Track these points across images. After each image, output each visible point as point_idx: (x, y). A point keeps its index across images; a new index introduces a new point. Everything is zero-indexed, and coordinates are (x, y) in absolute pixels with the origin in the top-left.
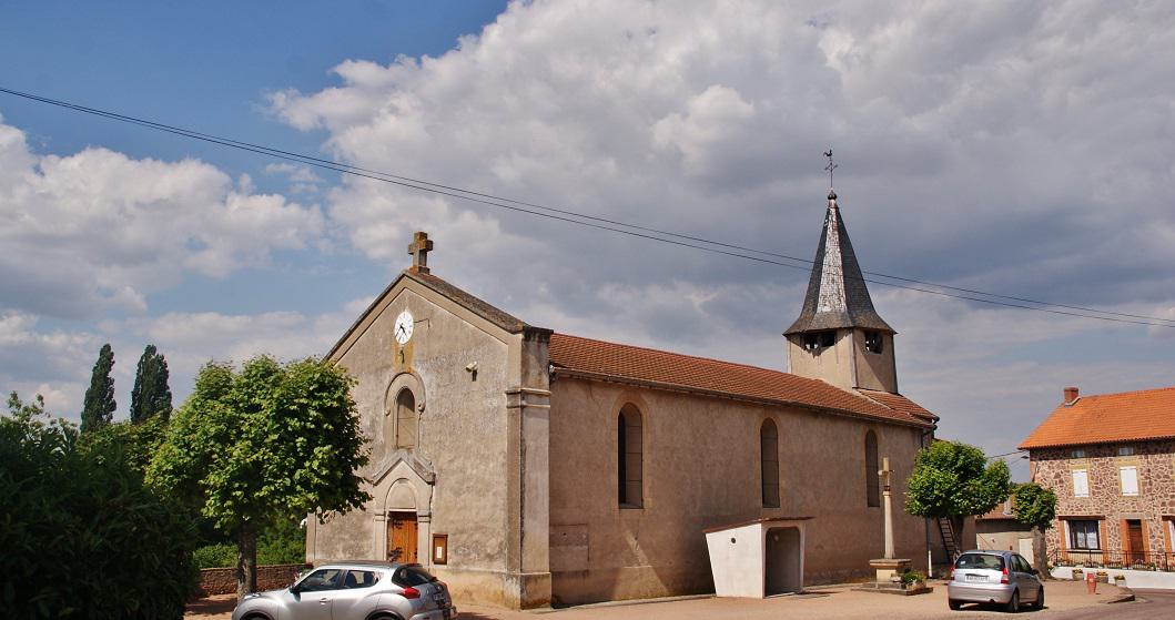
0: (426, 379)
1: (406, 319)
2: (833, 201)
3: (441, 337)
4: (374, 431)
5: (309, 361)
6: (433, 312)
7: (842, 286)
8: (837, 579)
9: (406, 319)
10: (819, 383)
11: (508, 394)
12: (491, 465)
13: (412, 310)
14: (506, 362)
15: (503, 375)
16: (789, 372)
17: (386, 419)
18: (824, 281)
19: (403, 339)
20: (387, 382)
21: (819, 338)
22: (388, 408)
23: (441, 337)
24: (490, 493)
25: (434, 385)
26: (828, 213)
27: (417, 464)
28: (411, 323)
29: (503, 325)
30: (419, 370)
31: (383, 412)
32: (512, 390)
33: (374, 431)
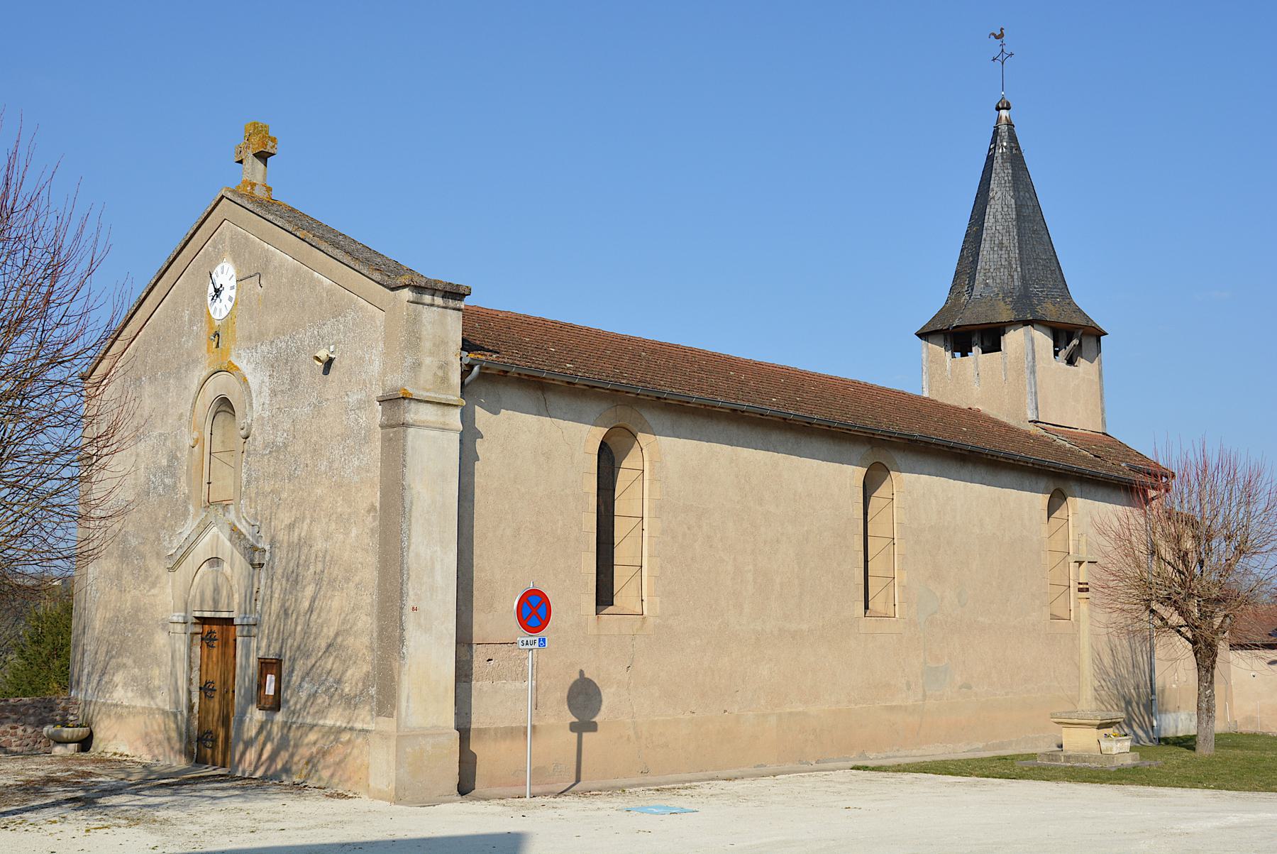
0: (254, 382)
1: (226, 274)
2: (1004, 113)
3: (278, 304)
4: (173, 475)
5: (899, 765)
6: (267, 260)
7: (1015, 254)
8: (1020, 778)
9: (226, 274)
10: (973, 414)
11: (382, 401)
12: (354, 532)
13: (236, 260)
14: (381, 344)
15: (376, 367)
16: (926, 394)
17: (191, 453)
18: (985, 246)
19: (220, 310)
20: (194, 387)
21: (975, 339)
22: (195, 435)
23: (278, 304)
24: (351, 585)
25: (266, 391)
26: (996, 132)
27: (234, 529)
28: (233, 282)
29: (377, 276)
30: (244, 366)
31: (188, 442)
32: (392, 394)
33: (173, 475)
